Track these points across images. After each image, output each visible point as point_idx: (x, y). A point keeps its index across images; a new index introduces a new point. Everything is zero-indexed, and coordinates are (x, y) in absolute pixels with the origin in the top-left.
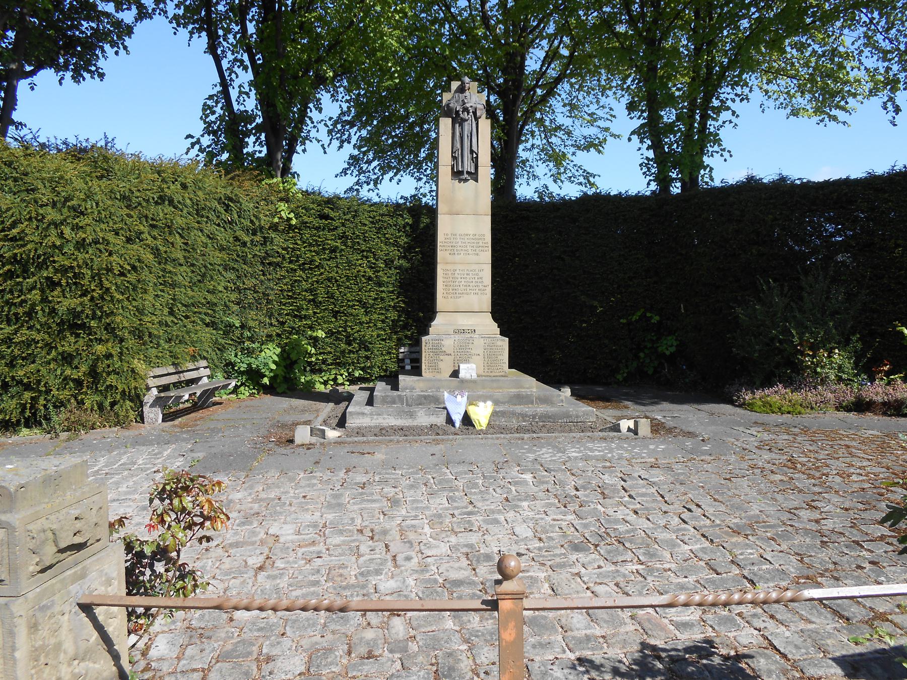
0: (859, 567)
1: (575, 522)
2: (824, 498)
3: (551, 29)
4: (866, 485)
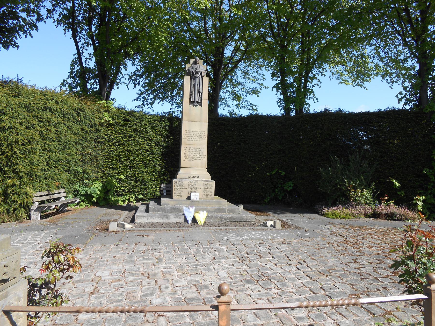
0: (378, 290)
1: (247, 270)
2: (361, 258)
3: (236, 37)
4: (380, 252)
